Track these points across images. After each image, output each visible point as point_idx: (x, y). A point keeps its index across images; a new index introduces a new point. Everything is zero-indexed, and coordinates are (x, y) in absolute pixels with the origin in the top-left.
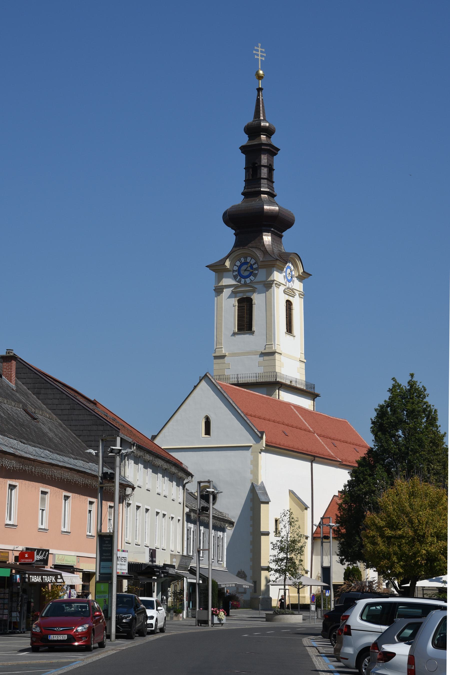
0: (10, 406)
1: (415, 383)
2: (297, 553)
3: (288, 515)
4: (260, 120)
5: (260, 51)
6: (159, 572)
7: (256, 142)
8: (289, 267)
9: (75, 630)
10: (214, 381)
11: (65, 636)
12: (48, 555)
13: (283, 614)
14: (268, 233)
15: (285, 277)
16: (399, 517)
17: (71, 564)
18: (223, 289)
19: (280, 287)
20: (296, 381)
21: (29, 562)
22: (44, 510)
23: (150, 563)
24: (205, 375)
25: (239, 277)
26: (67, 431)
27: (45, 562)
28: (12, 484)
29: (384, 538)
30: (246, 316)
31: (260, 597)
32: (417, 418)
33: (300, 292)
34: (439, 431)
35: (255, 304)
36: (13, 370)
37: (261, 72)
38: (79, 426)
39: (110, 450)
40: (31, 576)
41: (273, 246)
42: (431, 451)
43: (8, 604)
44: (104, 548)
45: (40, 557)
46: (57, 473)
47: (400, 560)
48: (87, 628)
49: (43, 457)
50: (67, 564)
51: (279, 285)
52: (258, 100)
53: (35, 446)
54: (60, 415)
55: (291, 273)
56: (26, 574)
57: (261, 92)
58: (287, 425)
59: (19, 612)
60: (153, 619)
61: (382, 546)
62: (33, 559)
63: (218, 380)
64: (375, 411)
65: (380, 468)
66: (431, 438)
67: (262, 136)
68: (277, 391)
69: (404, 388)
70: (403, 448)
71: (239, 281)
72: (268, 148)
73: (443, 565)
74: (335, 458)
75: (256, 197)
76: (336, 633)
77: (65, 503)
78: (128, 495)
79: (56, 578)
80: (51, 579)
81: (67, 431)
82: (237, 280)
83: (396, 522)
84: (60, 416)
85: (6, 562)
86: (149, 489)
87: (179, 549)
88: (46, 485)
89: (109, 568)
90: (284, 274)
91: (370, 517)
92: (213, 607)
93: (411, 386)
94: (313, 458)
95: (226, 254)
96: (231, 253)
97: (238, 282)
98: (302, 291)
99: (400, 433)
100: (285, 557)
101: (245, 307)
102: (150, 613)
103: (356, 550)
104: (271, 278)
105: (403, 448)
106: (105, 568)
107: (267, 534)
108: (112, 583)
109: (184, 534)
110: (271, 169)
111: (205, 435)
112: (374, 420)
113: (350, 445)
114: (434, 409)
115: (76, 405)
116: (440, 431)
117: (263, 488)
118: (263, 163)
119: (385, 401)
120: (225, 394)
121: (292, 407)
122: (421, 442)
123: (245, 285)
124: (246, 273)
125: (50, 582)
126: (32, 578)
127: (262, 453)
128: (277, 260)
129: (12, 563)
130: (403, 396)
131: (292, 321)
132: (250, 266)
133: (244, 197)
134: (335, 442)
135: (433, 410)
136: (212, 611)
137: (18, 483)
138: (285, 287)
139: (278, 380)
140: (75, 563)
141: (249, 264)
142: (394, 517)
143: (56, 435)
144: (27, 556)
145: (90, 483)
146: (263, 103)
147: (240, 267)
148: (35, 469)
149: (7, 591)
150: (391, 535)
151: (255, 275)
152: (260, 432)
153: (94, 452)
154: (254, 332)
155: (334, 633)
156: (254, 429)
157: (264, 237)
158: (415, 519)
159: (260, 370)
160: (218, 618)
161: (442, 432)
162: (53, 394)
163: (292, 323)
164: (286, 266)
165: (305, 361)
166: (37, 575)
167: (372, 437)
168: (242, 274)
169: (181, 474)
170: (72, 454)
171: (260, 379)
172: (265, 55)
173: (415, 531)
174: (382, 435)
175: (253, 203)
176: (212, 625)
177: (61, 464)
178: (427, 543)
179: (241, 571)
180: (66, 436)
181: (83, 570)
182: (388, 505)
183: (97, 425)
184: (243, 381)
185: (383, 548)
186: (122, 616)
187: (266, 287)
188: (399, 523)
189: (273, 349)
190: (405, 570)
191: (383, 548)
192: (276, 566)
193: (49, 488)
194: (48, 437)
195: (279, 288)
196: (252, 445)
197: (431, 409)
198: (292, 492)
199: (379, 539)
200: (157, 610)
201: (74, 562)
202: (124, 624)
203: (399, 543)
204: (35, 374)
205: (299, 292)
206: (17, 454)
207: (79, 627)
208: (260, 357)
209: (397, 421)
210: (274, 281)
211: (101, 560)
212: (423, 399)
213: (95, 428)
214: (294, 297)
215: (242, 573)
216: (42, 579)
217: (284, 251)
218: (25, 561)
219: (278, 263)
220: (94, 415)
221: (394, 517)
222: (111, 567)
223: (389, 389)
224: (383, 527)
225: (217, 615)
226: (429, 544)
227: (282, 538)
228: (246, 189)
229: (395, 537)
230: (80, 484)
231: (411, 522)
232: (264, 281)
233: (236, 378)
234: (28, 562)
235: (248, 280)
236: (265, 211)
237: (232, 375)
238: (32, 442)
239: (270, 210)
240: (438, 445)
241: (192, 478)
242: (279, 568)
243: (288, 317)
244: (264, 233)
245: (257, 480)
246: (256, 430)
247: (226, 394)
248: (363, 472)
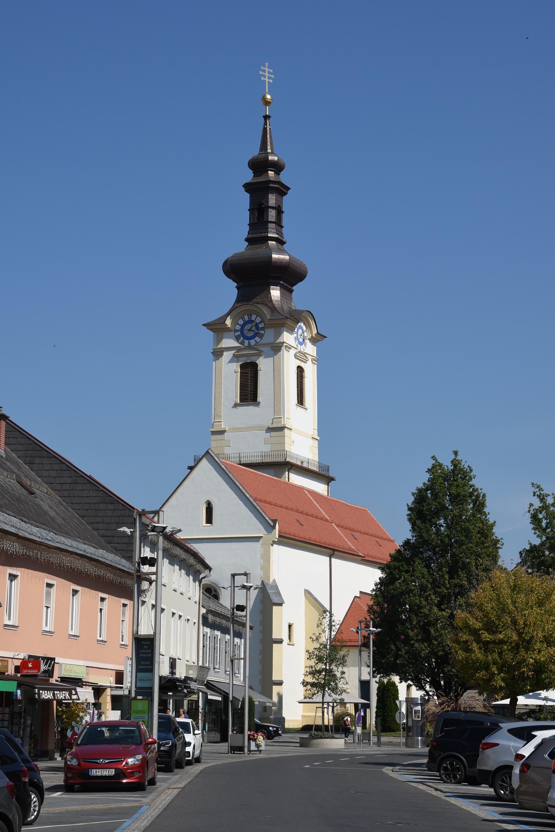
0: (1, 477)
1: (459, 462)
2: (339, 663)
3: (328, 618)
4: (267, 153)
5: (267, 72)
6: (181, 686)
7: (262, 179)
8: (301, 327)
9: (124, 763)
10: (217, 459)
11: (112, 770)
12: (53, 666)
13: (321, 738)
14: (277, 286)
15: (297, 338)
16: (499, 618)
17: (80, 676)
18: (223, 352)
19: (291, 351)
20: (308, 462)
21: (34, 673)
22: (49, 607)
23: (170, 676)
24: (207, 452)
25: (242, 338)
26: (69, 511)
27: (50, 673)
28: (12, 573)
29: (480, 643)
30: (250, 384)
31: (272, 717)
32: (462, 504)
33: (313, 357)
34: (488, 520)
35: (261, 370)
36: (2, 433)
37: (268, 97)
38: (82, 504)
39: (151, 528)
40: (41, 692)
41: (282, 302)
42: (480, 543)
43: (8, 727)
44: (141, 655)
45: (45, 667)
46: (67, 561)
47: (500, 670)
48: (141, 759)
49: (50, 541)
50: (75, 676)
51: (289, 347)
52: (265, 130)
53: (37, 526)
54: (59, 490)
55: (302, 335)
56: (35, 688)
57: (268, 120)
58: (302, 513)
59: (21, 738)
60: (190, 746)
61: (478, 654)
62: (39, 670)
63: (225, 459)
64: (413, 495)
65: (419, 563)
66: (479, 527)
67: (269, 172)
68: (287, 472)
69: (446, 468)
70: (446, 540)
71: (242, 343)
72: (277, 186)
73: (553, 677)
74: (356, 552)
75: (262, 244)
76: (447, 765)
77: (73, 599)
78: (145, 590)
79: (70, 694)
80: (64, 695)
81: (69, 511)
82: (240, 341)
83: (495, 624)
84: (58, 491)
85: (4, 673)
86: (165, 584)
87: (194, 659)
88: (52, 576)
89: (148, 681)
90: (295, 335)
91: (460, 618)
92: (250, 730)
93: (455, 466)
94: (332, 552)
95: (227, 311)
96: (232, 309)
97: (240, 343)
98: (315, 356)
99: (442, 521)
100: (324, 668)
101: (248, 373)
102: (189, 737)
103: (391, 661)
104: (280, 340)
105: (446, 540)
106: (143, 680)
107: (280, 641)
108: (152, 700)
109: (200, 640)
110: (279, 211)
111: (206, 523)
112: (410, 506)
113: (371, 537)
114: (482, 493)
115: (79, 478)
116: (489, 520)
117: (275, 587)
119: (424, 484)
120: (230, 475)
121: (306, 492)
122: (467, 533)
123: (250, 347)
124: (251, 334)
125: (63, 698)
126: (42, 693)
127: (274, 545)
128: (287, 318)
129: (11, 675)
130: (445, 478)
131: (304, 391)
132: (255, 326)
133: (247, 243)
134: (355, 534)
135: (482, 495)
136: (248, 734)
137: (20, 572)
138: (296, 351)
139: (287, 460)
140: (84, 675)
141: (254, 323)
142: (492, 617)
143: (58, 514)
144: (32, 666)
145: (103, 574)
146: (270, 133)
147: (243, 326)
148: (41, 555)
149: (7, 710)
150: (489, 639)
151: (261, 336)
152: (272, 520)
153: (128, 531)
154: (259, 403)
155: (444, 765)
156: (265, 517)
157: (271, 291)
158: (520, 619)
159: (266, 449)
160: (256, 743)
161: (491, 521)
162: (50, 464)
163: (304, 393)
164: (298, 325)
165: (318, 438)
166: (48, 689)
167: (409, 526)
169: (199, 567)
170: (79, 538)
171: (266, 459)
172: (273, 76)
173: (520, 634)
174: (422, 524)
175: (259, 251)
176: (249, 753)
177: (70, 549)
178: (535, 650)
180: (69, 516)
181: (97, 684)
182: (484, 603)
183: (106, 503)
184: (246, 461)
185: (479, 655)
186: (159, 742)
187: (273, 350)
188: (499, 625)
190: (507, 684)
191: (479, 655)
192: (313, 679)
193: (55, 580)
194: (49, 516)
195: (289, 352)
196: (263, 536)
197: (478, 493)
198: (308, 593)
199: (475, 644)
200: (194, 734)
201: (84, 674)
202: (161, 753)
203: (499, 650)
204: (28, 439)
205: (311, 357)
206: (20, 534)
207: (130, 757)
208: (266, 432)
209: (439, 507)
210: (283, 343)
211: (138, 670)
212: (469, 482)
213: (102, 506)
214: (306, 363)
216: (54, 694)
217: (294, 308)
218: (28, 673)
219: (289, 322)
220: (102, 490)
221: (492, 617)
222: (151, 680)
223: (428, 469)
224: (479, 630)
225: (255, 740)
226: (537, 650)
227: (321, 646)
228: (251, 234)
229: (494, 642)
230: (92, 576)
231: (514, 622)
232: (272, 343)
233: (238, 457)
234: (32, 673)
235: (253, 342)
236: (273, 260)
237: (233, 454)
238: (34, 521)
239: (279, 259)
240: (487, 536)
241: (210, 572)
242: (316, 681)
243: (299, 386)
244: (272, 287)
245: (269, 578)
246: (268, 518)
247: (232, 475)
248: (399, 568)
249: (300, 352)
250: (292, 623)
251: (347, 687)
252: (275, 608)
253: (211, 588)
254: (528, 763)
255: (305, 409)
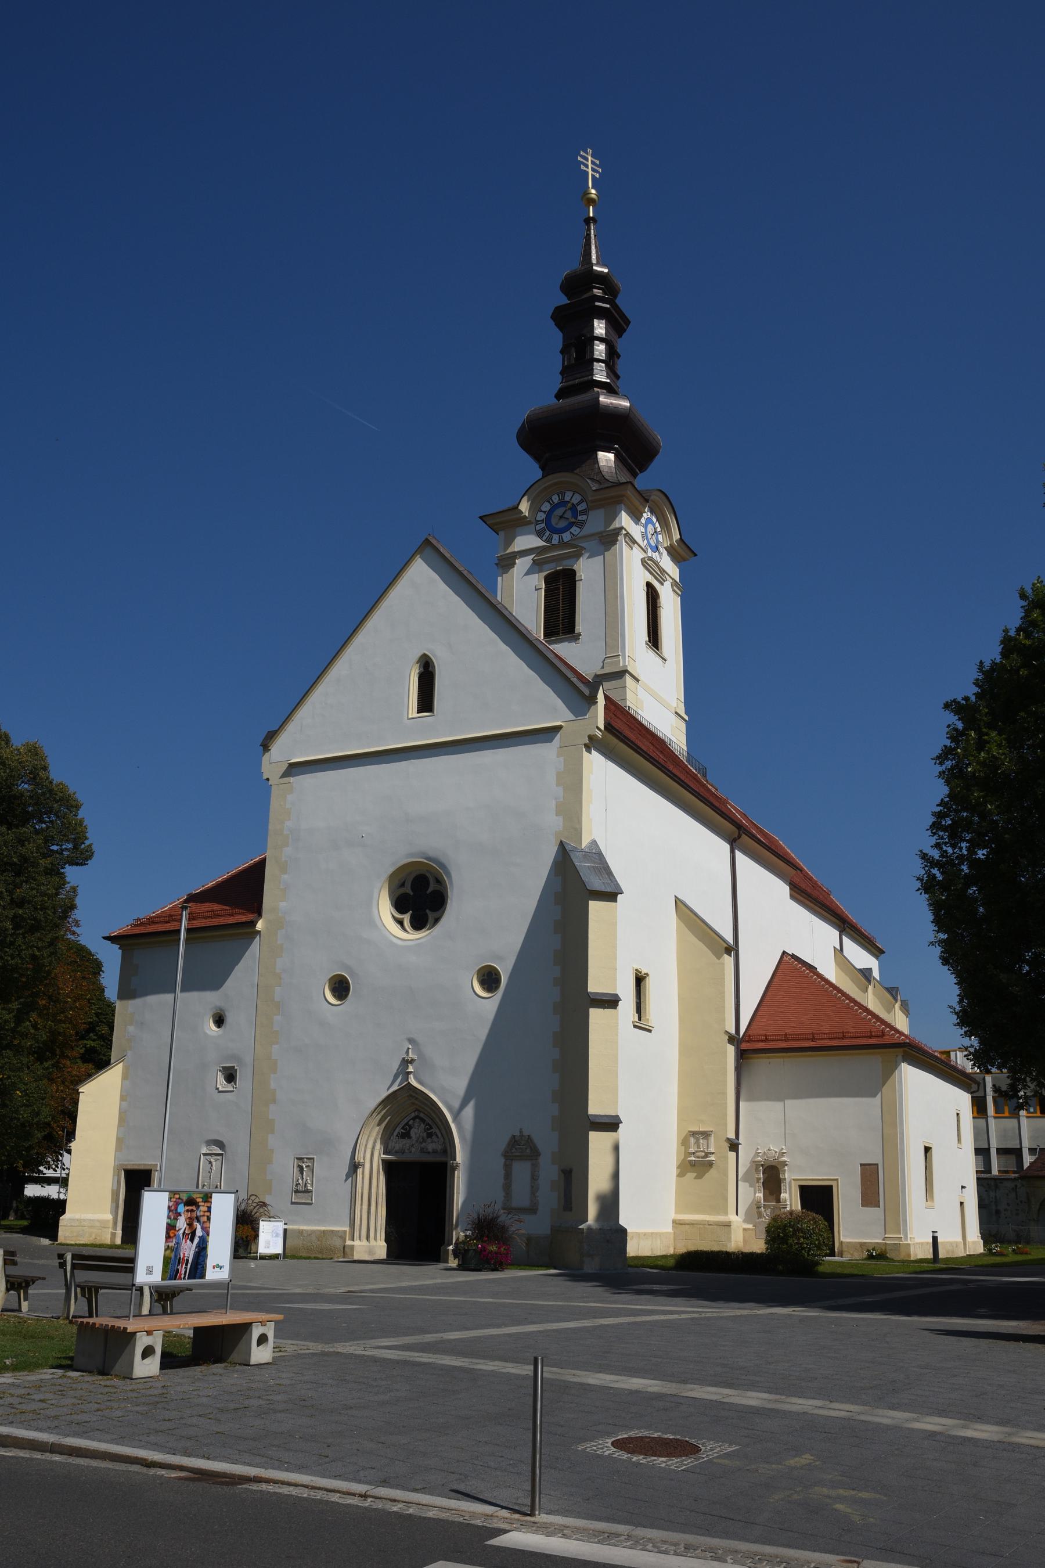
14: (610, 452)
25: (548, 533)
35: (581, 580)
82: (544, 538)
97: (545, 541)
99: (1000, 724)
104: (616, 525)
107: (611, 1002)
118: (597, 334)
123: (562, 545)
124: (563, 524)
147: (549, 514)
151: (581, 525)
154: (579, 634)
165: (686, 718)
168: (555, 526)
179: (522, 1136)
189: (621, 665)
210: (622, 528)
215: (523, 1143)
228: (564, 382)
232: (601, 533)
235: (566, 537)
249: (651, 559)
250: (644, 971)
251: (782, 1149)
252: (594, 906)
253: (428, 875)
254: (685, 1177)
255: (663, 658)
